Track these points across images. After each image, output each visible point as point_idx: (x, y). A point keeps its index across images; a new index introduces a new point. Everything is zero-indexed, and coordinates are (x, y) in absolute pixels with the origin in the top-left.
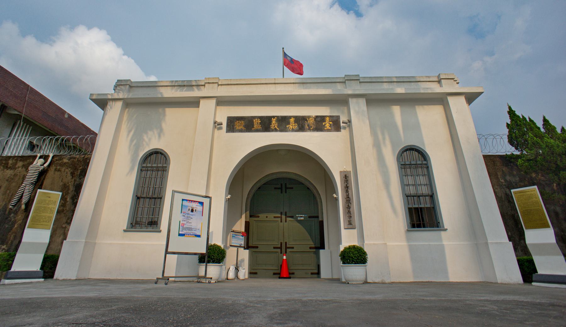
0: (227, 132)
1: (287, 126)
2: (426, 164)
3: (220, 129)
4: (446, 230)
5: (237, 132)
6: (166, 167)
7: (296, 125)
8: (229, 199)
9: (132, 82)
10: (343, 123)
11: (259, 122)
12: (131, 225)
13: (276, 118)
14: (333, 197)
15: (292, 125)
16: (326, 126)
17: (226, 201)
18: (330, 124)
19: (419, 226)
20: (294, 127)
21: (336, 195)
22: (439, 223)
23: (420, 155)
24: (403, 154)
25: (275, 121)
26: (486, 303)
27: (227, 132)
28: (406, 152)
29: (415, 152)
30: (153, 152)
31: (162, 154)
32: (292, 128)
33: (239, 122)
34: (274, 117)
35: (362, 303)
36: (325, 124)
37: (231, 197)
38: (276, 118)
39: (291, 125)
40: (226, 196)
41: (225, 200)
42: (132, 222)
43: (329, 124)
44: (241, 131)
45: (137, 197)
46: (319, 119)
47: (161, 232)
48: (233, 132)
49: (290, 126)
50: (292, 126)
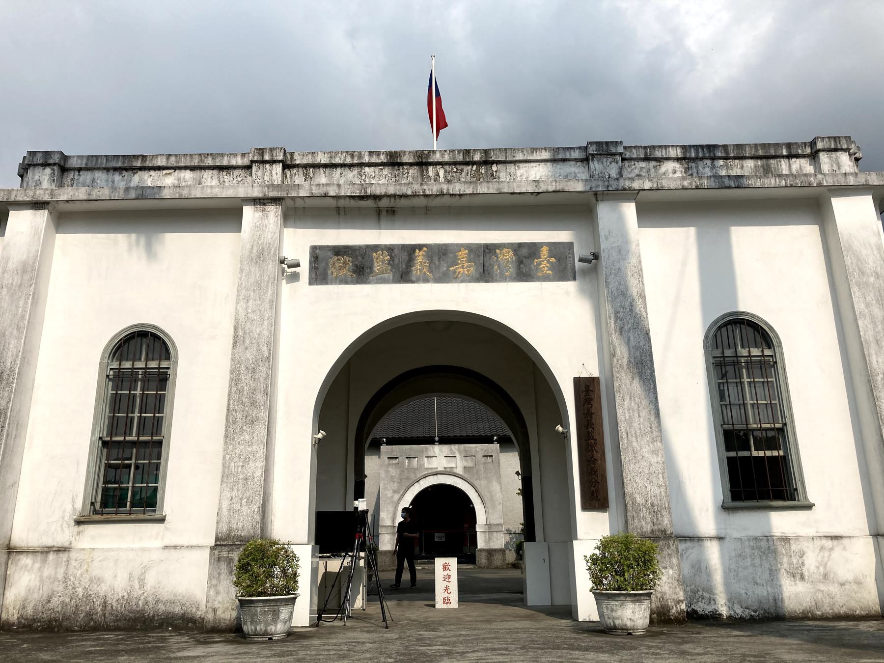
0: (310, 284)
1: (451, 269)
2: (771, 356)
3: (295, 277)
4: (809, 507)
5: (336, 283)
6: (168, 368)
7: (471, 266)
8: (319, 439)
9: (66, 156)
10: (581, 260)
11: (386, 258)
12: (92, 507)
13: (425, 249)
14: (557, 432)
15: (464, 266)
16: (541, 266)
17: (314, 445)
18: (552, 264)
19: (750, 497)
20: (468, 271)
21: (562, 426)
22: (796, 489)
23: (759, 333)
24: (719, 332)
25: (422, 255)
26: (99, 161)
27: (310, 284)
28: (725, 328)
29: (748, 328)
30: (135, 332)
31: (154, 336)
32: (462, 272)
33: (338, 259)
34: (420, 247)
35: (252, 162)
36: (539, 264)
37: (324, 437)
38: (425, 249)
39: (460, 265)
40: (316, 431)
41: (312, 442)
42: (93, 501)
43: (548, 262)
44: (344, 281)
45: (100, 442)
46: (524, 252)
47: (166, 522)
48: (327, 283)
49: (457, 268)
50: (462, 267)
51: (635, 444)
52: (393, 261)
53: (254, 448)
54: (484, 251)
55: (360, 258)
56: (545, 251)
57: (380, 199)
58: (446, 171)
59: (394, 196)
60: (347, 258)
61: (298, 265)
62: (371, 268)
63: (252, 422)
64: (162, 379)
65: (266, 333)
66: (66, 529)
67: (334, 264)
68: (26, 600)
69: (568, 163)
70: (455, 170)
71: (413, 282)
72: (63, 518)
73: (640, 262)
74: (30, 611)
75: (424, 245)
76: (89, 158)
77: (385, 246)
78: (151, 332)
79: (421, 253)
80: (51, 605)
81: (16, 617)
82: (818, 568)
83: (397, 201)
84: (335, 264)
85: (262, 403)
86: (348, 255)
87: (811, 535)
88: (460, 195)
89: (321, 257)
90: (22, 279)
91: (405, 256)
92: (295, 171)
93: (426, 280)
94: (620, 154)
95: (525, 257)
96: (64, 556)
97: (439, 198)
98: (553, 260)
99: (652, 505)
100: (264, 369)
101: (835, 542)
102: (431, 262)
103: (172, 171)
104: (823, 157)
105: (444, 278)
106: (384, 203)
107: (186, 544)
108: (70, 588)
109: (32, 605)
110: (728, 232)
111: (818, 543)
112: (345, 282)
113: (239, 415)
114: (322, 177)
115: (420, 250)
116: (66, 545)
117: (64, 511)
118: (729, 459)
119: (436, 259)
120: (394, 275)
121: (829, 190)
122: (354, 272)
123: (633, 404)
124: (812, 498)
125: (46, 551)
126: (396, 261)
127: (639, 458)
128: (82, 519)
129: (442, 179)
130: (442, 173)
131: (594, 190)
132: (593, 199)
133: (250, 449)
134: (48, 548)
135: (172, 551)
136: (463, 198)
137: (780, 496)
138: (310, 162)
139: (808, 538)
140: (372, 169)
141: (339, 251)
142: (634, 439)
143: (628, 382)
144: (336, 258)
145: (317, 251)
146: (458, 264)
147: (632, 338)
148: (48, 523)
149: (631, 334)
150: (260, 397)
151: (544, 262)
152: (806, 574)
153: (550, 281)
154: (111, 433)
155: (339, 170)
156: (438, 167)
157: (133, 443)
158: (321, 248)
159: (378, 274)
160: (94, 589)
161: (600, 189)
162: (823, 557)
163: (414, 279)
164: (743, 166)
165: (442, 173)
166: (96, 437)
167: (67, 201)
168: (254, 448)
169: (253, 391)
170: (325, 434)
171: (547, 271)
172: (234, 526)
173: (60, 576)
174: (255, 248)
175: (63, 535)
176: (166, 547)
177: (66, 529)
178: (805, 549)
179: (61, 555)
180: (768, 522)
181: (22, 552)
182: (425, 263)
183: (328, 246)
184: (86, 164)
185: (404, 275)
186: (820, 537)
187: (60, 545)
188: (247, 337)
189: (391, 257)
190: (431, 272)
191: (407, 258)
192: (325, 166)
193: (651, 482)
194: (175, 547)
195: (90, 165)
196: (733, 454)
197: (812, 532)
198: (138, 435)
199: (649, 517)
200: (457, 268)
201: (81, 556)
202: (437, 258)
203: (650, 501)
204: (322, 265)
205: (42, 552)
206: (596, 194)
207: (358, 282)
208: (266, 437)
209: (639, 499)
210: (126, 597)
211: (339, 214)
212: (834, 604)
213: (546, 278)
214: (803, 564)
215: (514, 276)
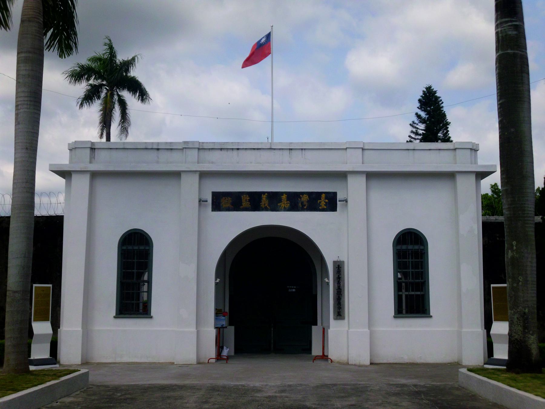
7: (288, 203)
13: (266, 194)
15: (285, 202)
25: (265, 197)
34: (264, 193)
36: (320, 202)
37: (220, 281)
38: (266, 194)
43: (325, 202)
50: (284, 204)
56: (284, 197)
60: (229, 198)
61: (207, 201)
69: (276, 150)
76: (185, 143)
78: (414, 232)
79: (265, 196)
98: (327, 201)
105: (274, 208)
110: (480, 181)
115: (264, 195)
118: (407, 312)
133: (513, 316)
146: (282, 202)
170: (219, 280)
171: (324, 206)
182: (266, 201)
200: (281, 204)
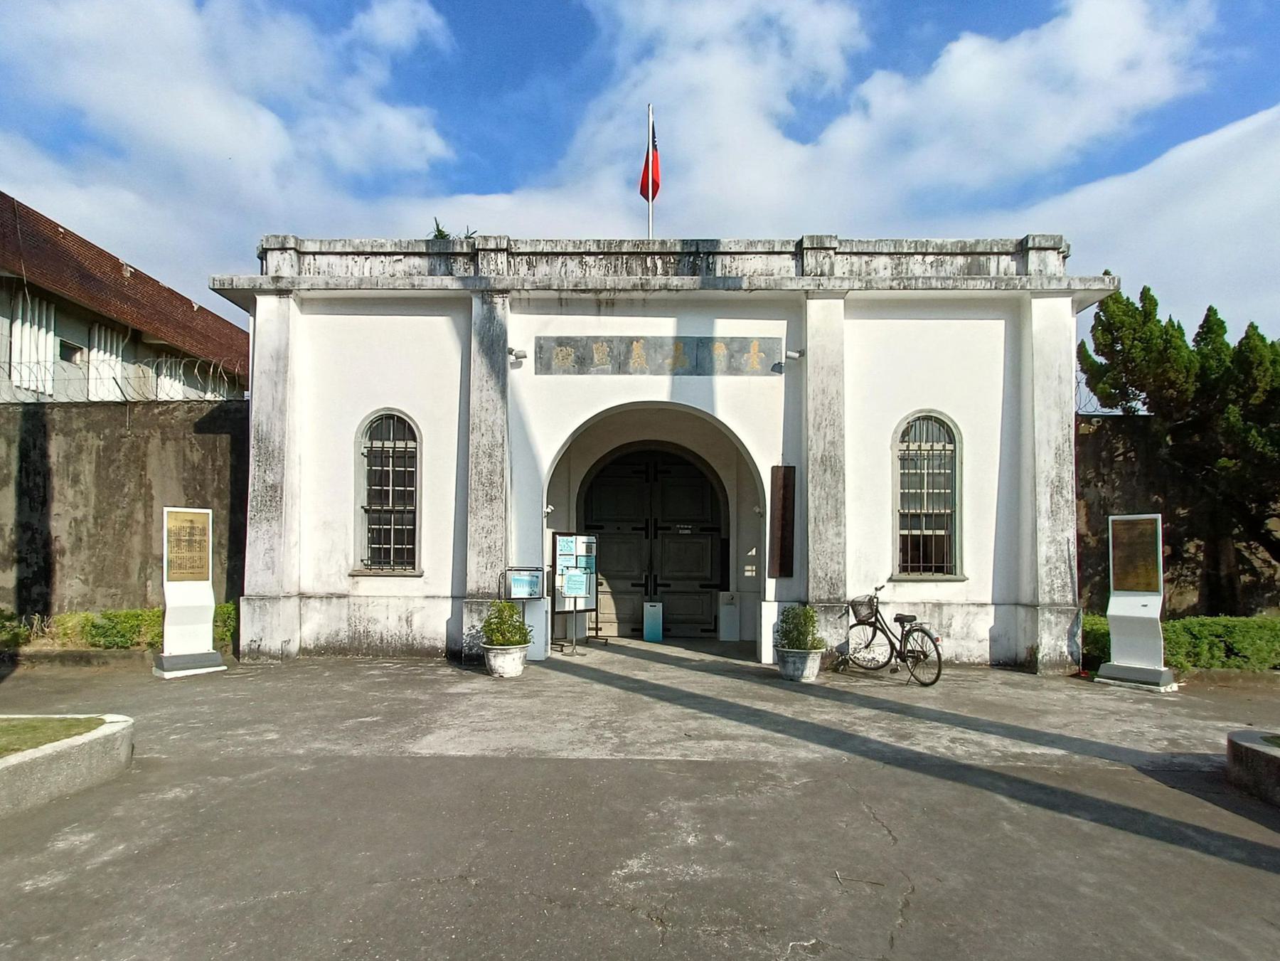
5: (559, 373)
13: (642, 341)
18: (761, 359)
34: (638, 339)
38: (642, 341)
48: (551, 374)
51: (821, 527)
52: (612, 352)
53: (495, 522)
54: (698, 345)
55: (581, 349)
56: (754, 347)
57: (600, 293)
58: (663, 263)
59: (614, 290)
62: (592, 359)
63: (491, 500)
64: (410, 458)
65: (499, 422)
66: (343, 580)
67: (557, 355)
68: (318, 634)
70: (672, 261)
71: (630, 374)
72: (340, 571)
73: (843, 362)
74: (322, 641)
75: (642, 338)
77: (605, 337)
80: (339, 638)
81: (312, 646)
82: (962, 628)
83: (617, 294)
84: (559, 353)
85: (499, 484)
86: (571, 347)
87: (961, 603)
88: (677, 290)
89: (545, 347)
90: (278, 366)
91: (623, 348)
92: (518, 259)
93: (643, 372)
94: (835, 249)
95: (736, 352)
96: (344, 601)
97: (656, 292)
99: (831, 578)
100: (499, 454)
101: (980, 609)
102: (648, 354)
103: (402, 257)
104: (1033, 256)
106: (604, 295)
107: (442, 595)
108: (353, 625)
109: (325, 636)
111: (966, 608)
112: (566, 372)
113: (480, 493)
114: (543, 268)
116: (346, 593)
117: (340, 566)
119: (652, 351)
120: (613, 367)
121: (1031, 293)
122: (577, 363)
123: (823, 493)
124: (967, 572)
125: (329, 597)
126: (615, 352)
127: (824, 538)
128: (355, 573)
129: (660, 271)
130: (659, 263)
131: (805, 288)
132: (804, 297)
133: (491, 523)
134: (332, 594)
135: (431, 599)
136: (680, 292)
137: (939, 570)
138: (533, 250)
139: (958, 604)
140: (593, 258)
141: (562, 342)
142: (821, 523)
143: (820, 473)
144: (559, 349)
145: (542, 342)
147: (828, 434)
148: (328, 575)
149: (827, 430)
150: (496, 478)
151: (753, 358)
152: (952, 632)
153: (758, 375)
154: (369, 503)
155: (560, 259)
156: (656, 257)
157: (390, 512)
158: (546, 339)
159: (598, 365)
160: (371, 628)
161: (812, 288)
162: (968, 620)
163: (631, 371)
164: (952, 262)
165: (659, 263)
166: (359, 507)
167: (309, 290)
168: (495, 522)
169: (491, 473)
172: (482, 585)
173: (345, 616)
174: (485, 340)
175: (344, 585)
176: (427, 597)
177: (343, 580)
178: (955, 614)
179: (342, 600)
180: (673, 392)
181: (310, 597)
183: (552, 337)
184: (320, 248)
185: (621, 367)
186: (969, 604)
187: (340, 592)
188: (483, 425)
189: (610, 348)
190: (647, 364)
191: (625, 350)
192: (547, 254)
193: (832, 560)
194: (433, 597)
195: (324, 250)
196: (905, 532)
197: (962, 600)
198: (393, 506)
199: (827, 587)
201: (358, 601)
202: (653, 350)
203: (829, 575)
204: (545, 356)
205: (327, 598)
206: (807, 292)
207: (579, 373)
208: (505, 426)
209: (820, 574)
210: (398, 634)
211: (561, 305)
212: (971, 656)
213: (754, 373)
214: (950, 625)
215: (725, 369)
